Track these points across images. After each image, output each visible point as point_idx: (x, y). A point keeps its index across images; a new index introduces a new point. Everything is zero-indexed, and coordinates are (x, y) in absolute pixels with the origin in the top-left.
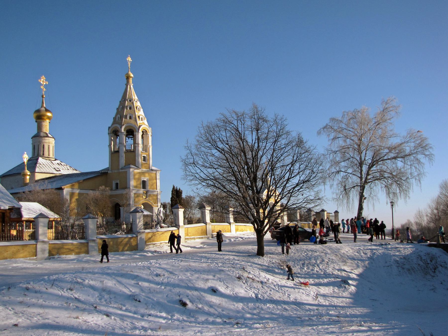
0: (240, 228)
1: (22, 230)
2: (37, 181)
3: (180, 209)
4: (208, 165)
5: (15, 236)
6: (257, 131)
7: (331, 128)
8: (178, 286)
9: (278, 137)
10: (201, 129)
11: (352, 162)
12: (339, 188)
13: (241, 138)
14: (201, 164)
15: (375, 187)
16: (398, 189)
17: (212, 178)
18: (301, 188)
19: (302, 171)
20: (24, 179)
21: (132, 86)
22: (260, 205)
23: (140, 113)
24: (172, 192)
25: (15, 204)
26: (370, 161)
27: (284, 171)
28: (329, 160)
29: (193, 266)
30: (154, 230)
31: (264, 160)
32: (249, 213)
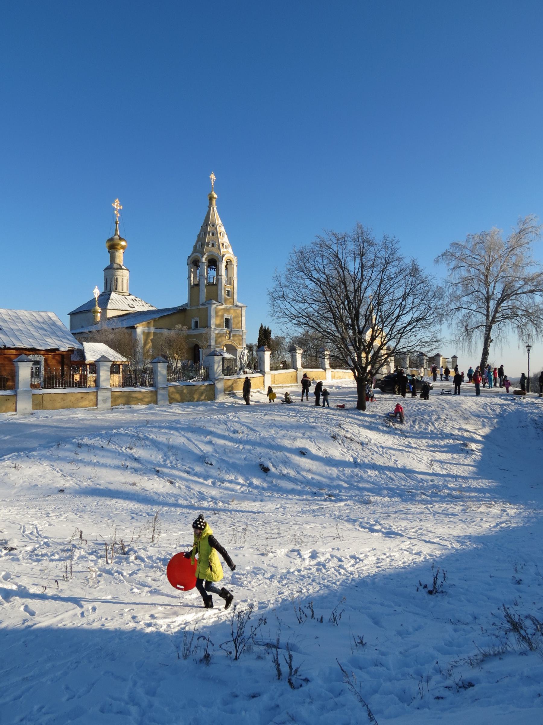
0: (337, 375)
1: (86, 375)
2: (109, 319)
3: (266, 352)
4: (300, 299)
5: (78, 381)
6: (362, 256)
7: (452, 255)
8: (260, 444)
9: (387, 264)
10: (292, 255)
11: (477, 297)
12: (459, 328)
13: (341, 266)
14: (292, 297)
15: (504, 328)
16: (534, 330)
17: (305, 314)
18: (414, 327)
19: (415, 307)
20: (95, 317)
21: (215, 209)
22: (362, 347)
23: (224, 240)
24: (260, 331)
25: (76, 346)
26: (499, 296)
27: (393, 307)
28: (447, 293)
29: (279, 421)
30: (235, 377)
31: (369, 293)
32: (349, 357)
